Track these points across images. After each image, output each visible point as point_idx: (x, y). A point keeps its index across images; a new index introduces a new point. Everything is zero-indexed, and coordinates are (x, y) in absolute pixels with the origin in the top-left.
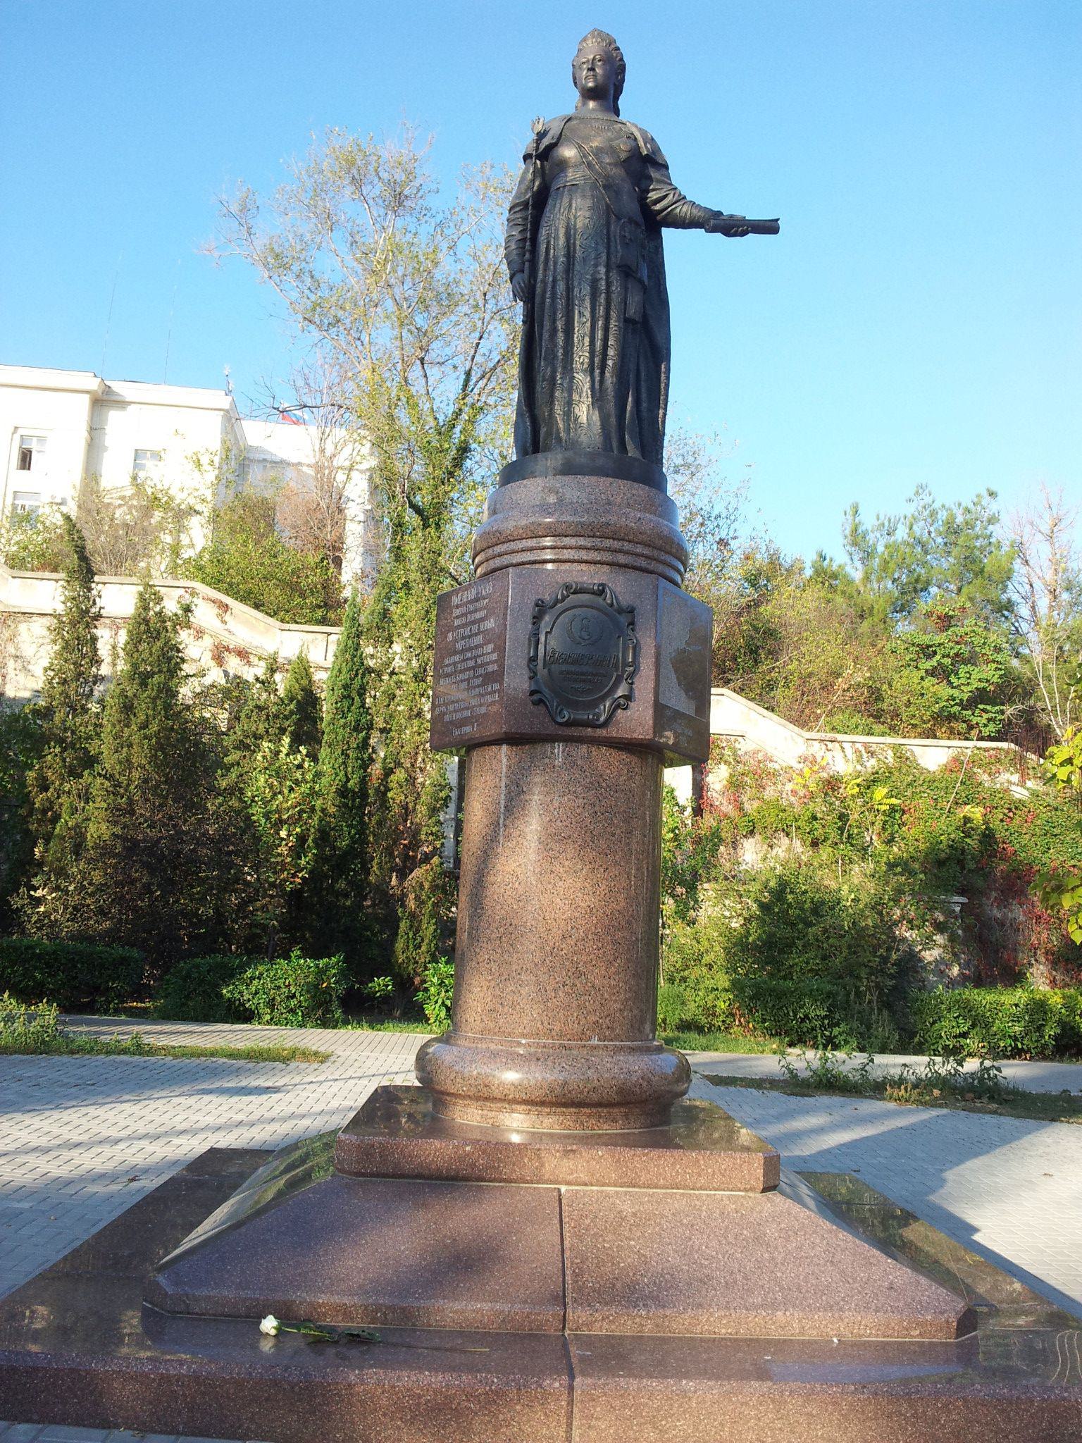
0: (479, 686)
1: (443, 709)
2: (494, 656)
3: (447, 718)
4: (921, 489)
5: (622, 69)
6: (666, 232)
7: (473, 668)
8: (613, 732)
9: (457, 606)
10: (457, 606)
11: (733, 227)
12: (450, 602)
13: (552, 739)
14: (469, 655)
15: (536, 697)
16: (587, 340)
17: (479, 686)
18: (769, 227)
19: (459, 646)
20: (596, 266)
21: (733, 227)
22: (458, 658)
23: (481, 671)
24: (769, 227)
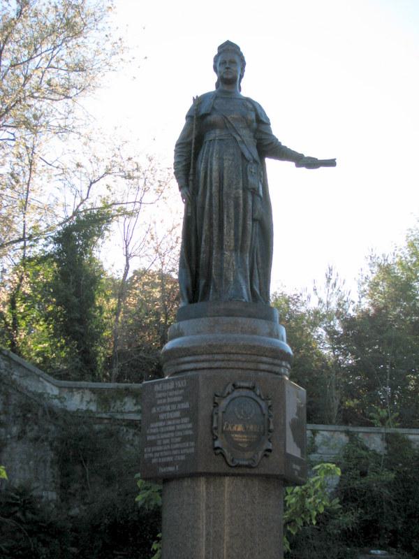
0: (178, 443)
1: (151, 455)
2: (190, 426)
3: (154, 461)
4: (147, 155)
5: (214, 59)
6: (270, 163)
7: (174, 431)
8: (262, 471)
9: (159, 392)
10: (159, 392)
11: (312, 163)
12: (153, 388)
13: (226, 475)
14: (170, 423)
15: (218, 451)
16: (232, 232)
17: (178, 443)
18: (331, 163)
19: (162, 417)
20: (237, 188)
21: (312, 163)
22: (161, 424)
23: (180, 434)
24: (331, 163)
